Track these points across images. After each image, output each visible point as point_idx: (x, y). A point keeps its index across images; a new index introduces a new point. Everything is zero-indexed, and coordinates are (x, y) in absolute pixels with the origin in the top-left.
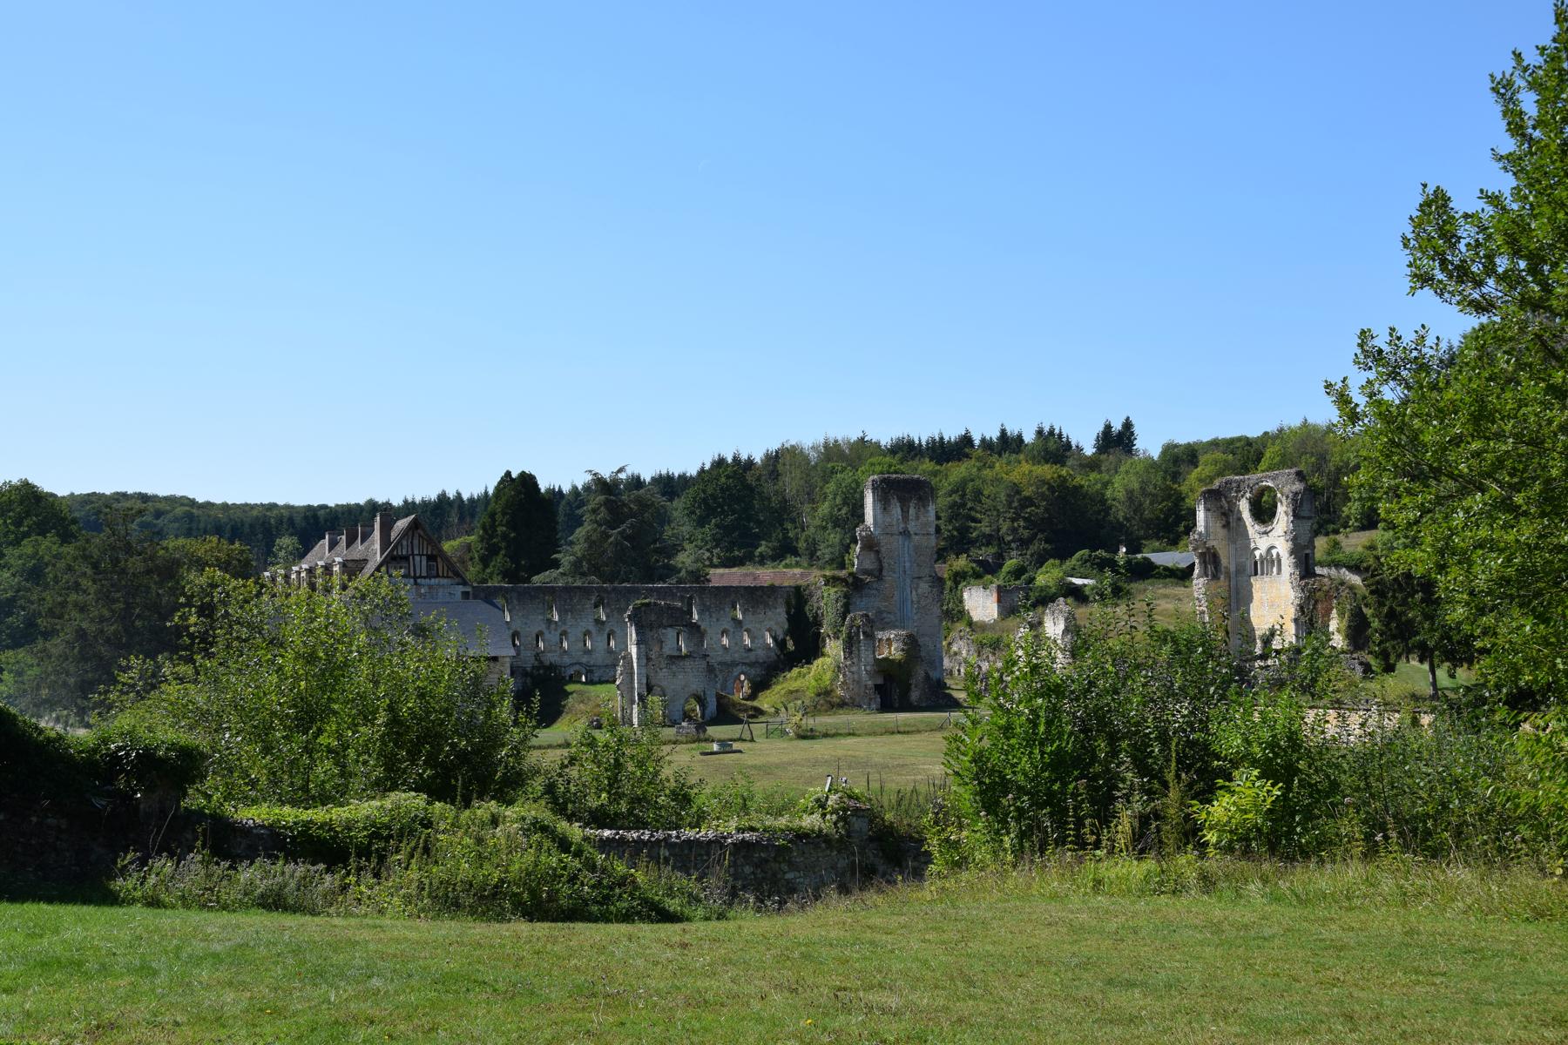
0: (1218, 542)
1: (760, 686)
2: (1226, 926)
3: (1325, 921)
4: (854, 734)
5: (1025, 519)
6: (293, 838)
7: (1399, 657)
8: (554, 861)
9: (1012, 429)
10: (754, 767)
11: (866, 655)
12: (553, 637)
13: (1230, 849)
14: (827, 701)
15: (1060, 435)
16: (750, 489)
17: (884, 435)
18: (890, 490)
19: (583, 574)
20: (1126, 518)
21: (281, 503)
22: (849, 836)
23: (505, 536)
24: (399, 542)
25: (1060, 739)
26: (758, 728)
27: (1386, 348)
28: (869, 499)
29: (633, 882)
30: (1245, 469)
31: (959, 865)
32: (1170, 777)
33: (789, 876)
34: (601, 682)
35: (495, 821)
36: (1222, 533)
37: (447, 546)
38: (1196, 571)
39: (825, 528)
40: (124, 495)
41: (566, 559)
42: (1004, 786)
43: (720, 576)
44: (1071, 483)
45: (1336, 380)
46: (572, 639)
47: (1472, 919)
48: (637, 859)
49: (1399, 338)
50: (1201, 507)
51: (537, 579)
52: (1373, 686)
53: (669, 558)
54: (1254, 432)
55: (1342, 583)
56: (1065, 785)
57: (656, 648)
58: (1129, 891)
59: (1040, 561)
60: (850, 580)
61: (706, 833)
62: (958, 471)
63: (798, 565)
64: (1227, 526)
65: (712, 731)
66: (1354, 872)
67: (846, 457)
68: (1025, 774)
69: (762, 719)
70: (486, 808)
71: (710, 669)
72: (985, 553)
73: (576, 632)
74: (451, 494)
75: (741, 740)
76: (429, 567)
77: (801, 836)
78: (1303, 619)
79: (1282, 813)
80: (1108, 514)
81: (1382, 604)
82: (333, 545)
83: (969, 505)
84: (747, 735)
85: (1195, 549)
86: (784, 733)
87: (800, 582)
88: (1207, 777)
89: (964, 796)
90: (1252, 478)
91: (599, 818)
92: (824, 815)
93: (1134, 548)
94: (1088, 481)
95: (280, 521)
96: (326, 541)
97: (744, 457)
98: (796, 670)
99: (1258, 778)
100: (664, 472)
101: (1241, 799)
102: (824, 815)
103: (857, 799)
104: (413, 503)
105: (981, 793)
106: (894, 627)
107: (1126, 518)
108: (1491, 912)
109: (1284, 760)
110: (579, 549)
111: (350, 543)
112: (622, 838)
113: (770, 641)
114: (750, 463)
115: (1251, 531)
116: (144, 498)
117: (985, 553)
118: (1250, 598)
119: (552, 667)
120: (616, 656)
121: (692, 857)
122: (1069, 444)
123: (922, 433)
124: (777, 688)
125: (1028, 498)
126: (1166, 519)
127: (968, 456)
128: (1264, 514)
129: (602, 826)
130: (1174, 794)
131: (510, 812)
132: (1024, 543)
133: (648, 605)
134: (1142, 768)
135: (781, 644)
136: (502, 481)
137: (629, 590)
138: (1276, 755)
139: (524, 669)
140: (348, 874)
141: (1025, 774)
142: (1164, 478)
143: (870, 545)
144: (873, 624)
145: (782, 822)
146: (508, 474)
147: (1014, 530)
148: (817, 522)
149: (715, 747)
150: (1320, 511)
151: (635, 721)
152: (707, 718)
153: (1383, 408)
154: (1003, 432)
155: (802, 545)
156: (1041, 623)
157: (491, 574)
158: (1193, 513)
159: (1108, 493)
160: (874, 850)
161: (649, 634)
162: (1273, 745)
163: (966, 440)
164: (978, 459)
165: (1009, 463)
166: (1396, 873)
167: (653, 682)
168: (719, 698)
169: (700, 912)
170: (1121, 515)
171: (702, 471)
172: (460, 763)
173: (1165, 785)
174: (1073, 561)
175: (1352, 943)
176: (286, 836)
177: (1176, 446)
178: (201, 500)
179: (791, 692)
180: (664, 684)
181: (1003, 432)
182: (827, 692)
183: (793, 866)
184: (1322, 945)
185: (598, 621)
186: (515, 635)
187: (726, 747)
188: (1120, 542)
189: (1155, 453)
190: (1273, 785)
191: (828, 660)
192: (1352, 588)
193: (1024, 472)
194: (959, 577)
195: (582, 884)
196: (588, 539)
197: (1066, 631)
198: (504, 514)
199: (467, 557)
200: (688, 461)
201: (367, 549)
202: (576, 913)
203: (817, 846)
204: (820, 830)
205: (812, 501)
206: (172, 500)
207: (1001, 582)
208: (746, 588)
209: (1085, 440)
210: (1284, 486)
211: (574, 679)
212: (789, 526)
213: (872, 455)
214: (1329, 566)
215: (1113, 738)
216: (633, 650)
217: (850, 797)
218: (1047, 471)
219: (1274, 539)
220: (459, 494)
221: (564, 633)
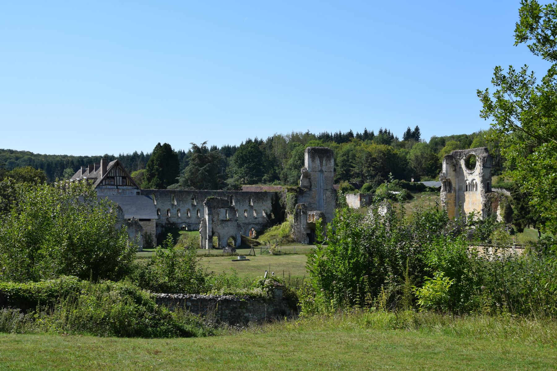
0: (452, 177)
1: (260, 233)
2: (420, 347)
3: (466, 345)
4: (297, 254)
5: (373, 167)
6: (11, 296)
7: (525, 226)
8: (131, 308)
9: (369, 130)
10: (254, 266)
11: (303, 221)
12: (174, 211)
13: (429, 309)
14: (287, 240)
15: (389, 133)
16: (260, 152)
17: (317, 131)
18: (314, 153)
19: (188, 186)
20: (415, 167)
21: (69, 155)
22: (274, 297)
23: (157, 170)
24: (110, 171)
25: (357, 257)
26: (257, 251)
27: (507, 76)
28: (306, 157)
29: (170, 317)
30: (464, 148)
31: (313, 312)
32: (406, 274)
33: (246, 315)
34: (194, 230)
35: (109, 289)
36: (453, 173)
37: (133, 174)
38: (442, 189)
39: (291, 169)
41: (181, 179)
42: (333, 278)
43: (247, 188)
44: (392, 152)
45: (483, 90)
46: (182, 212)
47: (537, 345)
48: (180, 308)
49: (514, 71)
50: (445, 162)
51: (169, 188)
52: (513, 237)
53: (225, 180)
54: (469, 133)
55: (503, 195)
56: (359, 277)
57: (216, 217)
58: (382, 327)
59: (379, 183)
60: (298, 190)
62: (346, 147)
63: (279, 184)
64: (455, 170)
65: (238, 251)
66: (484, 321)
67: (300, 140)
68: (341, 272)
69: (260, 247)
70: (105, 283)
71: (239, 226)
72: (355, 181)
73: (184, 210)
74: (139, 153)
75: (250, 255)
76: (123, 181)
77: (252, 297)
78: (486, 210)
79: (455, 291)
80: (407, 165)
81: (518, 204)
82: (84, 172)
83: (350, 161)
84: (252, 253)
85: (441, 180)
87: (277, 191)
88: (421, 273)
89: (312, 280)
90: (467, 150)
92: (263, 288)
93: (417, 179)
94: (400, 152)
95: (68, 162)
96: (81, 170)
97: (259, 139)
98: (274, 227)
99: (444, 276)
100: (227, 145)
101: (436, 287)
102: (263, 288)
103: (278, 281)
104: (123, 156)
105: (323, 280)
106: (316, 210)
107: (415, 167)
108: (546, 342)
109: (455, 269)
110: (187, 175)
111: (91, 171)
112: (170, 297)
113: (264, 214)
114: (262, 142)
115: (464, 172)
116: (11, 152)
117: (355, 181)
118: (464, 201)
119: (174, 224)
120: (200, 219)
121: (200, 306)
122: (393, 136)
123: (332, 131)
124: (266, 234)
125: (375, 158)
126: (431, 167)
127: (350, 141)
128: (471, 166)
130: (407, 283)
131: (115, 285)
132: (373, 177)
133: (213, 199)
134: (396, 272)
135: (269, 216)
136: (157, 147)
137: (206, 193)
138: (453, 266)
139: (162, 224)
140: (35, 313)
141: (341, 272)
142: (431, 151)
143: (307, 176)
144: (306, 209)
145: (244, 291)
146: (159, 144)
147: (369, 171)
148: (288, 167)
149: (239, 258)
150: (494, 165)
151: (207, 246)
152: (237, 246)
153: (502, 103)
154: (366, 131)
155: (281, 176)
157: (152, 185)
158: (441, 165)
159: (408, 157)
160: (281, 304)
161: (213, 211)
162: (451, 262)
164: (355, 142)
165: (367, 144)
166: (506, 321)
168: (242, 238)
169: (201, 331)
170: (412, 166)
171: (242, 145)
172: (99, 262)
173: (404, 279)
175: (476, 358)
176: (7, 296)
177: (437, 138)
178: (35, 153)
179: (272, 236)
180: (219, 231)
181: (366, 131)
182: (287, 236)
183: (248, 310)
184: (462, 357)
185: (193, 205)
186: (158, 210)
187: (243, 258)
188: (412, 177)
189: (428, 141)
190: (450, 280)
191: (288, 223)
192: (507, 197)
193: (373, 147)
194: (345, 190)
195: (146, 318)
196: (190, 171)
198: (157, 161)
199: (142, 178)
200: (236, 141)
201: (97, 173)
202: (141, 332)
203: (259, 302)
204: (261, 295)
205: (286, 158)
206: (23, 153)
207: (362, 192)
208: (255, 192)
209: (399, 135)
210: (479, 154)
211: (183, 229)
212: (276, 168)
213: (311, 140)
214: (498, 188)
215: (382, 258)
216: (207, 217)
217: (275, 281)
218: (382, 147)
219: (475, 176)
220: (142, 153)
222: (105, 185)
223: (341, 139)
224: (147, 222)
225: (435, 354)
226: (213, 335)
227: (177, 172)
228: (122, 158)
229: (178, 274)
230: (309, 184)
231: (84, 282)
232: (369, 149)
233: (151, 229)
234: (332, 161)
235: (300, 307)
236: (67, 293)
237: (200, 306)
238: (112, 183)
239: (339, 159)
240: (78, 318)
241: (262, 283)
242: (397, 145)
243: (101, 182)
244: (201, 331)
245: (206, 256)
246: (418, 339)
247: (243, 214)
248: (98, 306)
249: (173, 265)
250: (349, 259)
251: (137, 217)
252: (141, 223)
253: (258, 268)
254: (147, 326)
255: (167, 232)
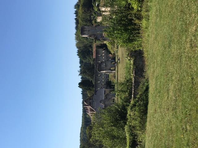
1: (110, 53)
10: (122, 56)
16: (82, 51)
17: (74, 31)
18: (82, 33)
19: (93, 77)
22: (134, 56)
23: (88, 87)
25: (122, 29)
26: (116, 54)
35: (130, 115)
40: (80, 136)
42: (129, 38)
43: (94, 56)
61: (133, 79)
62: (80, 21)
63: (93, 45)
65: (116, 61)
67: (78, 38)
71: (107, 60)
74: (81, 92)
77: (134, 64)
84: (117, 56)
86: (117, 50)
91: (130, 94)
96: (87, 113)
98: (108, 48)
103: (129, 54)
114: (78, 50)
116: (81, 134)
119: (106, 82)
120: (105, 74)
121: (137, 83)
122: (77, 4)
123: (75, 25)
129: (131, 97)
132: (91, 12)
135: (104, 50)
136: (79, 87)
143: (90, 36)
149: (119, 61)
154: (75, 13)
156: (103, 11)
163: (76, 19)
164: (78, 18)
167: (109, 69)
171: (79, 57)
172: (121, 116)
173: (130, 13)
174: (94, 5)
178: (81, 126)
181: (75, 13)
187: (119, 60)
193: (80, 11)
196: (88, 76)
197: (104, 7)
200: (77, 59)
206: (81, 130)
211: (108, 79)
215: (122, 20)
216: (104, 72)
217: (128, 55)
218: (80, 8)
221: (102, 81)
223: (77, 22)
224: (106, 92)
225: (160, 10)
226: (148, 78)
227: (88, 81)
228: (83, 98)
229: (125, 89)
231: (127, 123)
232: (81, 13)
233: (108, 91)
234: (85, 27)
235: (139, 49)
236: (131, 129)
237: (137, 83)
239: (85, 23)
240: (140, 127)
241: (129, 60)
242: (80, 2)
243: (91, 107)
244: (146, 84)
245: (118, 72)
246: (154, 13)
247: (103, 59)
248: (136, 120)
249: (122, 91)
250: (122, 32)
251: (104, 95)
252: (106, 94)
253: (122, 55)
254: (144, 103)
255: (110, 85)
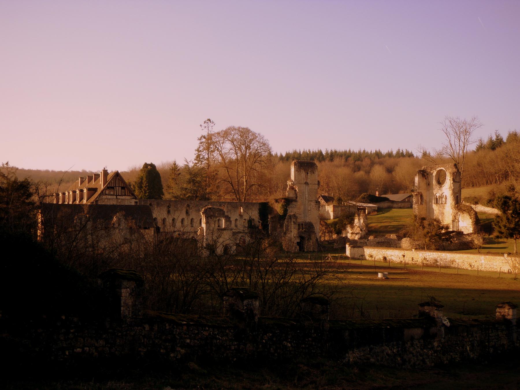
222: (106, 194)
230: (294, 196)
238: (112, 193)
243: (102, 192)
